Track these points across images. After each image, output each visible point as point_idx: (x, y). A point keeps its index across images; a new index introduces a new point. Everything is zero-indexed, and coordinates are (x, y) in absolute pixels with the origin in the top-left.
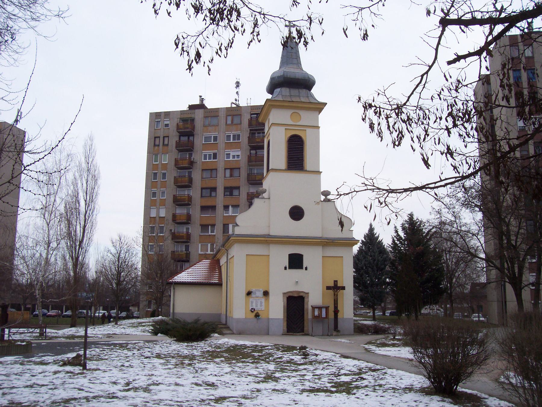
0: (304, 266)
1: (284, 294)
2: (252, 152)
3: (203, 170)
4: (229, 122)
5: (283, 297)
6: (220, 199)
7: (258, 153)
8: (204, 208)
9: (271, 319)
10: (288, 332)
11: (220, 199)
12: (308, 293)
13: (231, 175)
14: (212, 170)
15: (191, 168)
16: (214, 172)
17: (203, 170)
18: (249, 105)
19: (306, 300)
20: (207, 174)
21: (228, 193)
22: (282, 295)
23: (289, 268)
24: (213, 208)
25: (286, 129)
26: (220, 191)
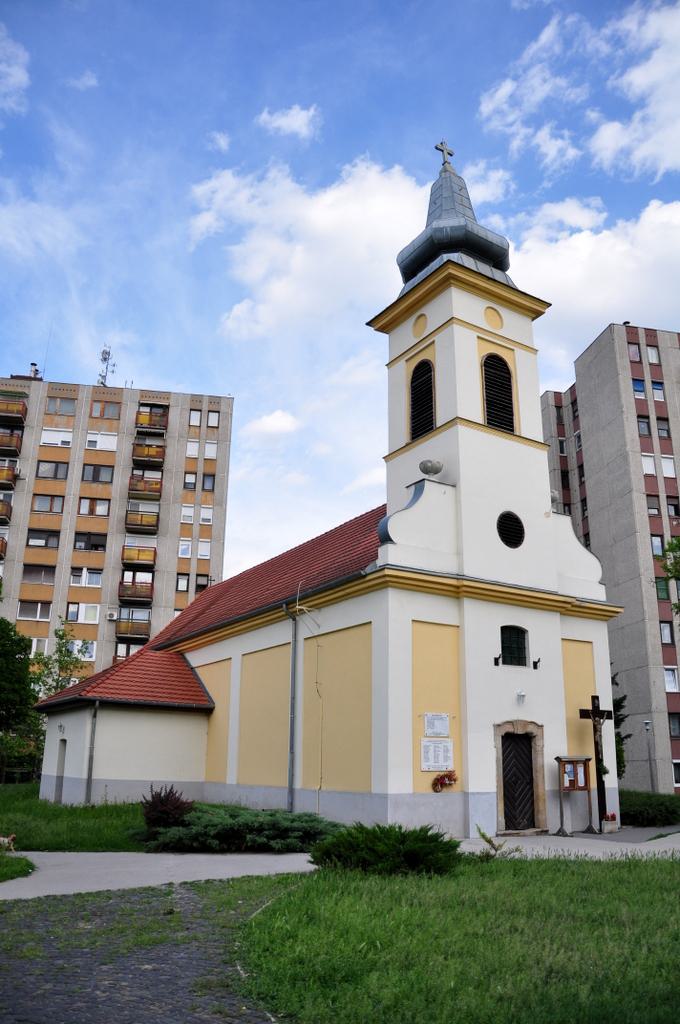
0: (532, 657)
1: (498, 726)
2: (135, 472)
3: (35, 495)
4: (96, 414)
5: (495, 735)
6: (66, 553)
7: (146, 475)
8: (30, 569)
9: (473, 794)
10: (508, 827)
11: (66, 553)
12: (542, 726)
13: (92, 511)
14: (53, 497)
15: (11, 488)
16: (57, 503)
17: (35, 495)
18: (128, 386)
19: (537, 743)
20: (42, 505)
21: (83, 545)
22: (492, 731)
23: (504, 663)
24: (50, 570)
25: (479, 337)
26: (67, 539)
